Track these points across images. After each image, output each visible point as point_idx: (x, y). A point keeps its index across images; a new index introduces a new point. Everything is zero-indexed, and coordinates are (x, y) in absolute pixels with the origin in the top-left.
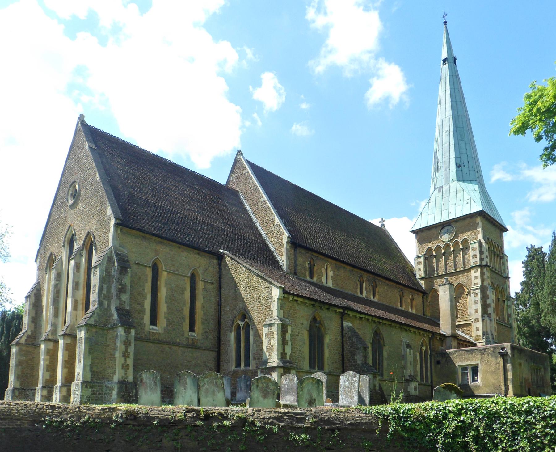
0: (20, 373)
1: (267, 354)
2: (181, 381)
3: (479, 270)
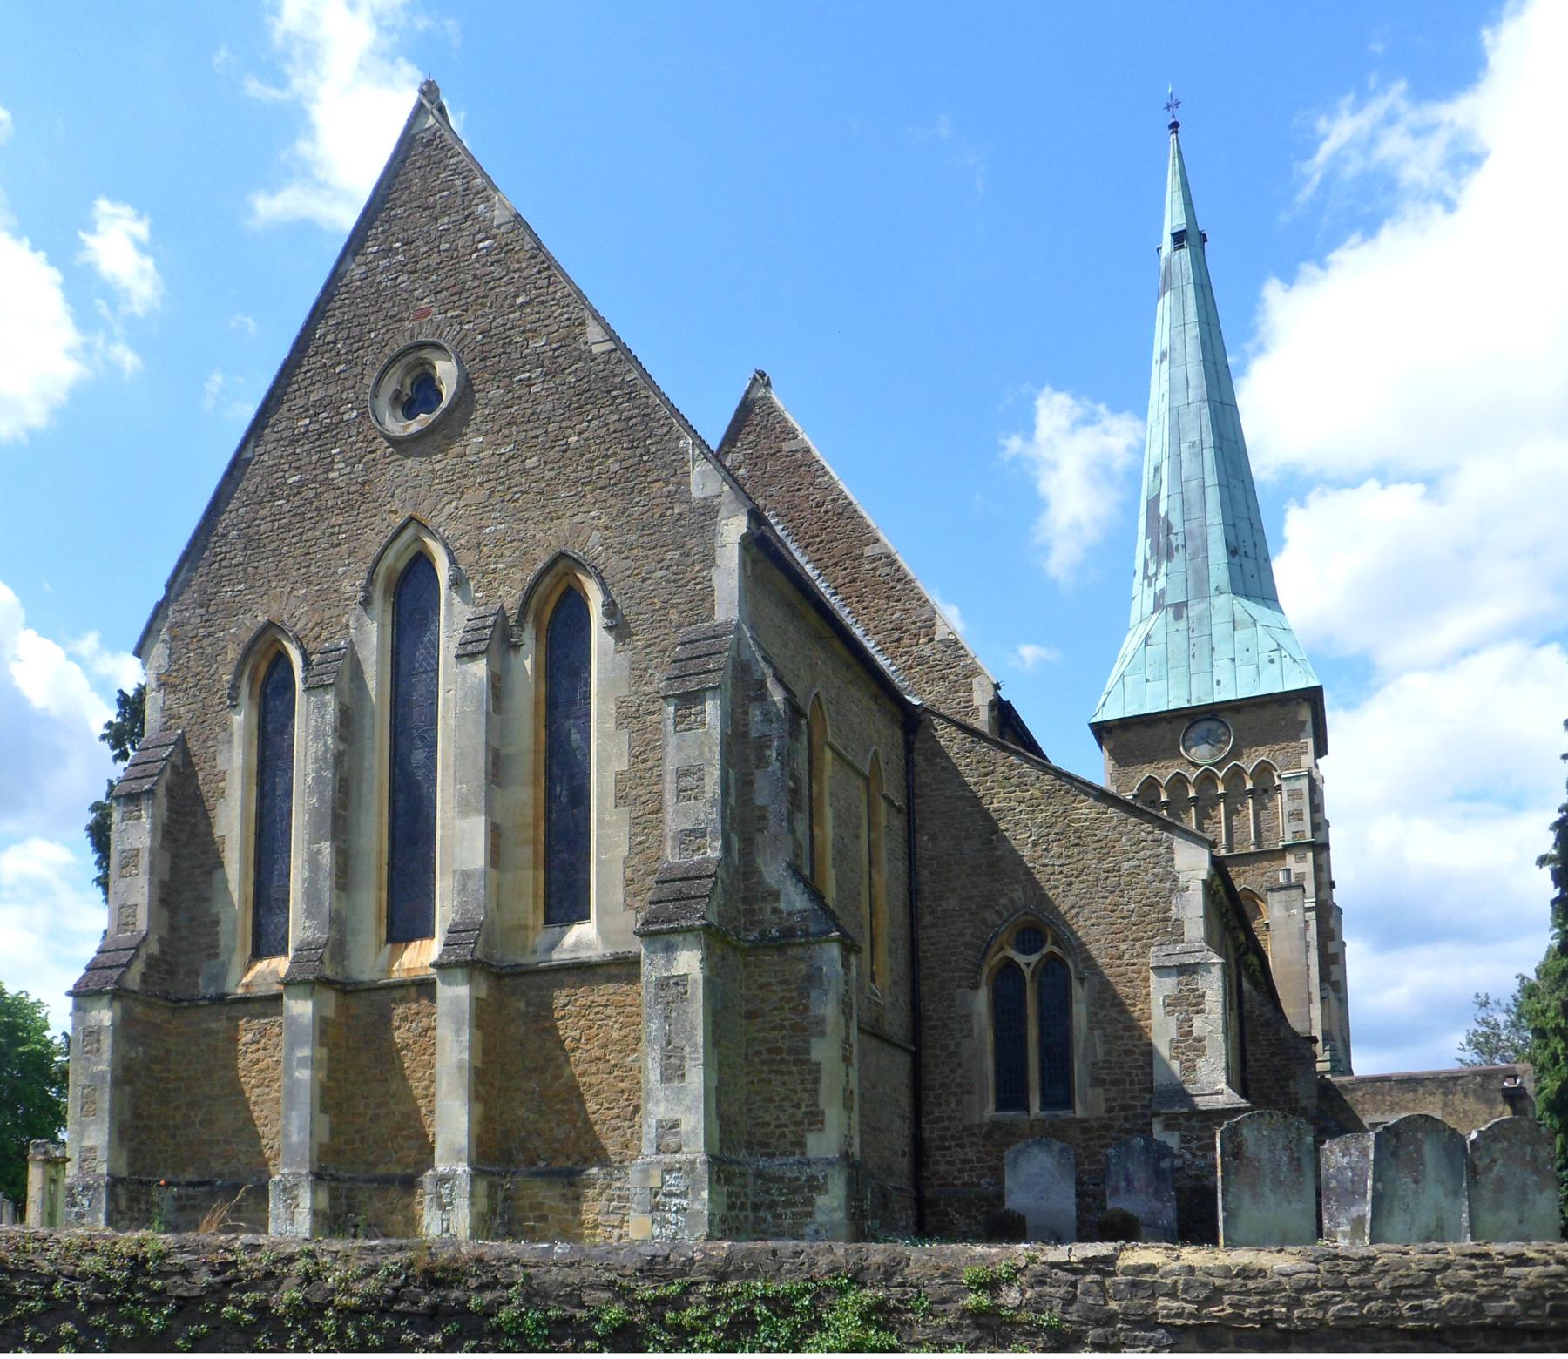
0: (127, 1116)
1: (1175, 1066)
2: (1401, 1152)
3: (1310, 855)
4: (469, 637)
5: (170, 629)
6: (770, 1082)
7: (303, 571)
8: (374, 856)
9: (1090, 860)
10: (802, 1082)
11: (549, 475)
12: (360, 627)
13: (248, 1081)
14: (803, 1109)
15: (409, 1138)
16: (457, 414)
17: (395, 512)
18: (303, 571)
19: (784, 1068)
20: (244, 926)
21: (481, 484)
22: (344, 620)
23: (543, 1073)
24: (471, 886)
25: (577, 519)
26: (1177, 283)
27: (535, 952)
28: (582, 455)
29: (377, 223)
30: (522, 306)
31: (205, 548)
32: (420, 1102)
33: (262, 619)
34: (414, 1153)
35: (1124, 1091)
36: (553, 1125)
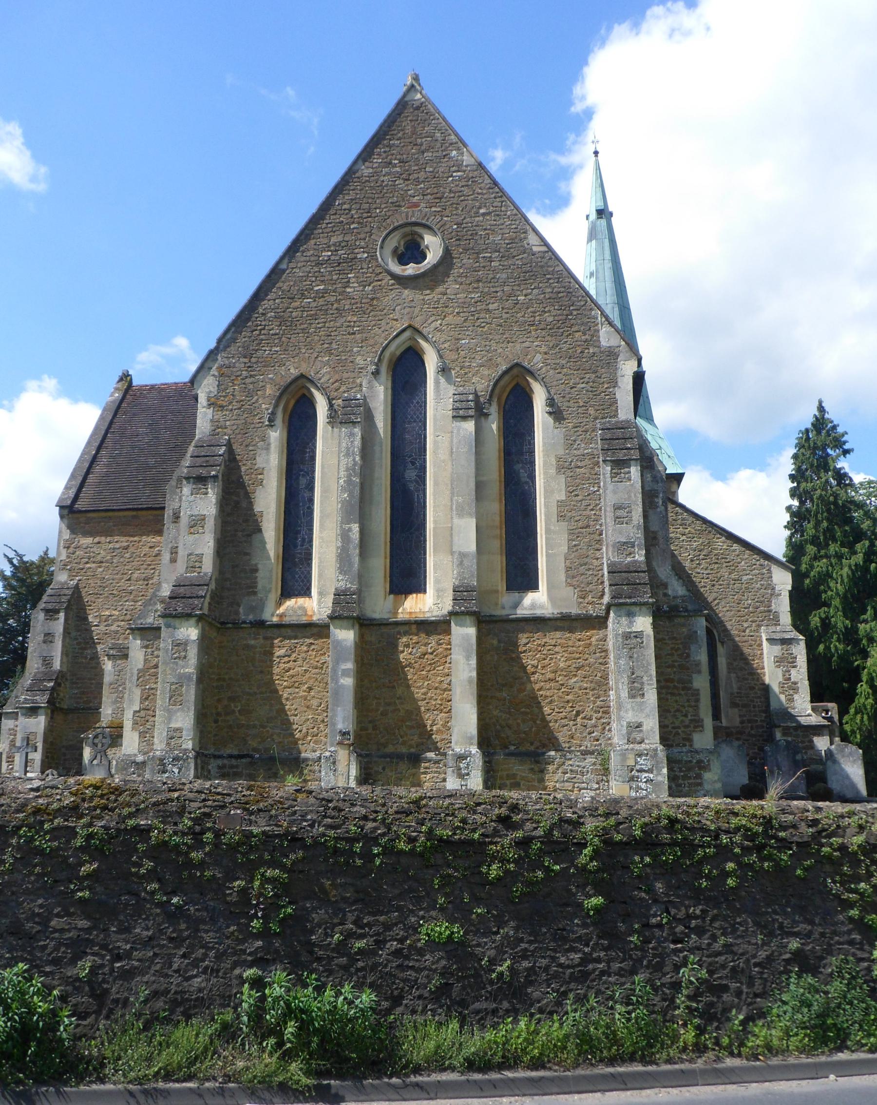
1: (783, 697)
4: (458, 405)
5: (220, 368)
6: (667, 700)
7: (326, 346)
8: (383, 536)
9: (724, 572)
10: (688, 701)
11: (505, 316)
12: (371, 387)
13: (281, 684)
14: (690, 718)
15: (412, 727)
16: (441, 269)
17: (396, 320)
18: (326, 346)
19: (676, 691)
20: (277, 574)
21: (458, 313)
22: (358, 381)
23: (512, 687)
24: (466, 563)
25: (527, 344)
26: (599, 236)
27: (503, 608)
28: (528, 308)
29: (380, 146)
30: (484, 214)
31: (248, 320)
32: (420, 703)
33: (294, 372)
34: (416, 738)
35: (750, 711)
36: (519, 721)
